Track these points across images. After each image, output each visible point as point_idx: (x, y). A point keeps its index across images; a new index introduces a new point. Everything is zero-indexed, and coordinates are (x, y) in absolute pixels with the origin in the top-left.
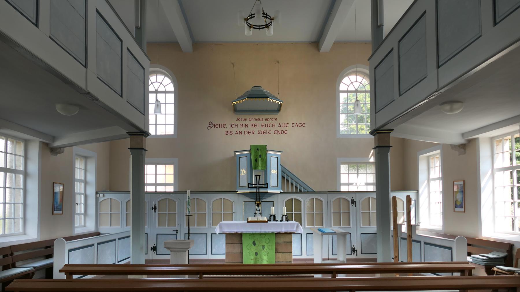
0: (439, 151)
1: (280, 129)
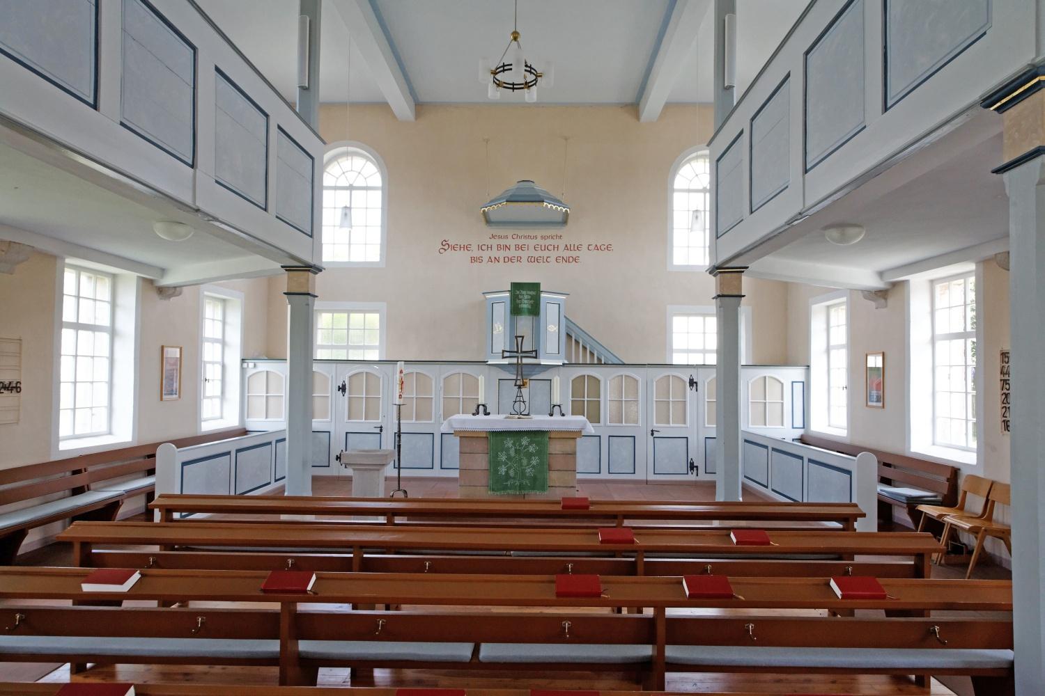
0: (844, 299)
1: (567, 254)
